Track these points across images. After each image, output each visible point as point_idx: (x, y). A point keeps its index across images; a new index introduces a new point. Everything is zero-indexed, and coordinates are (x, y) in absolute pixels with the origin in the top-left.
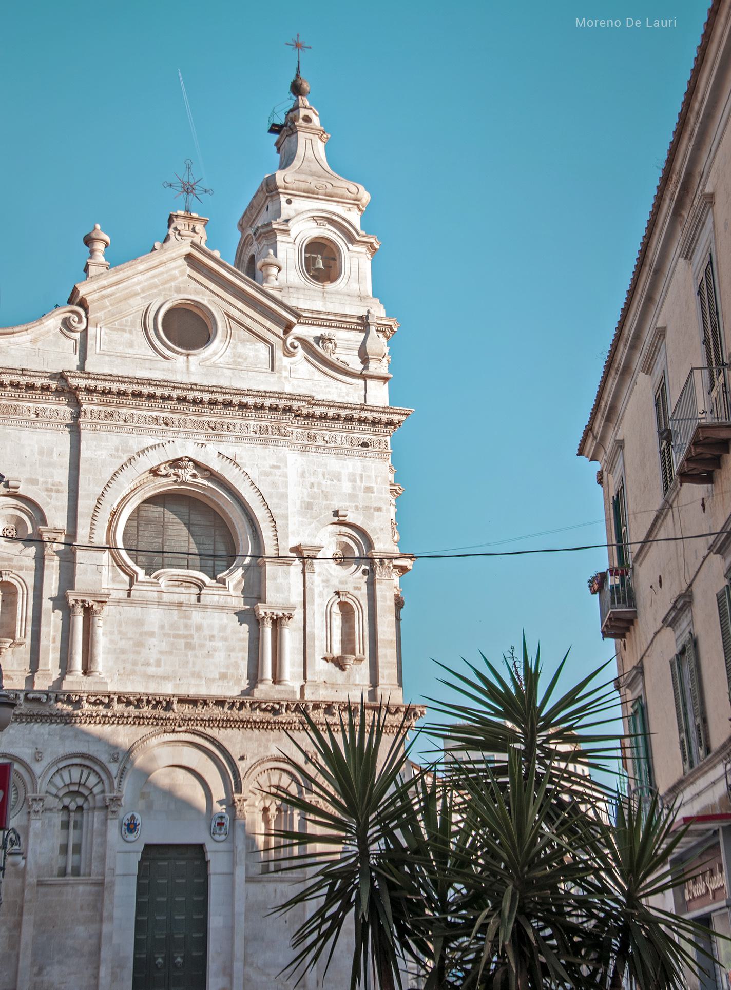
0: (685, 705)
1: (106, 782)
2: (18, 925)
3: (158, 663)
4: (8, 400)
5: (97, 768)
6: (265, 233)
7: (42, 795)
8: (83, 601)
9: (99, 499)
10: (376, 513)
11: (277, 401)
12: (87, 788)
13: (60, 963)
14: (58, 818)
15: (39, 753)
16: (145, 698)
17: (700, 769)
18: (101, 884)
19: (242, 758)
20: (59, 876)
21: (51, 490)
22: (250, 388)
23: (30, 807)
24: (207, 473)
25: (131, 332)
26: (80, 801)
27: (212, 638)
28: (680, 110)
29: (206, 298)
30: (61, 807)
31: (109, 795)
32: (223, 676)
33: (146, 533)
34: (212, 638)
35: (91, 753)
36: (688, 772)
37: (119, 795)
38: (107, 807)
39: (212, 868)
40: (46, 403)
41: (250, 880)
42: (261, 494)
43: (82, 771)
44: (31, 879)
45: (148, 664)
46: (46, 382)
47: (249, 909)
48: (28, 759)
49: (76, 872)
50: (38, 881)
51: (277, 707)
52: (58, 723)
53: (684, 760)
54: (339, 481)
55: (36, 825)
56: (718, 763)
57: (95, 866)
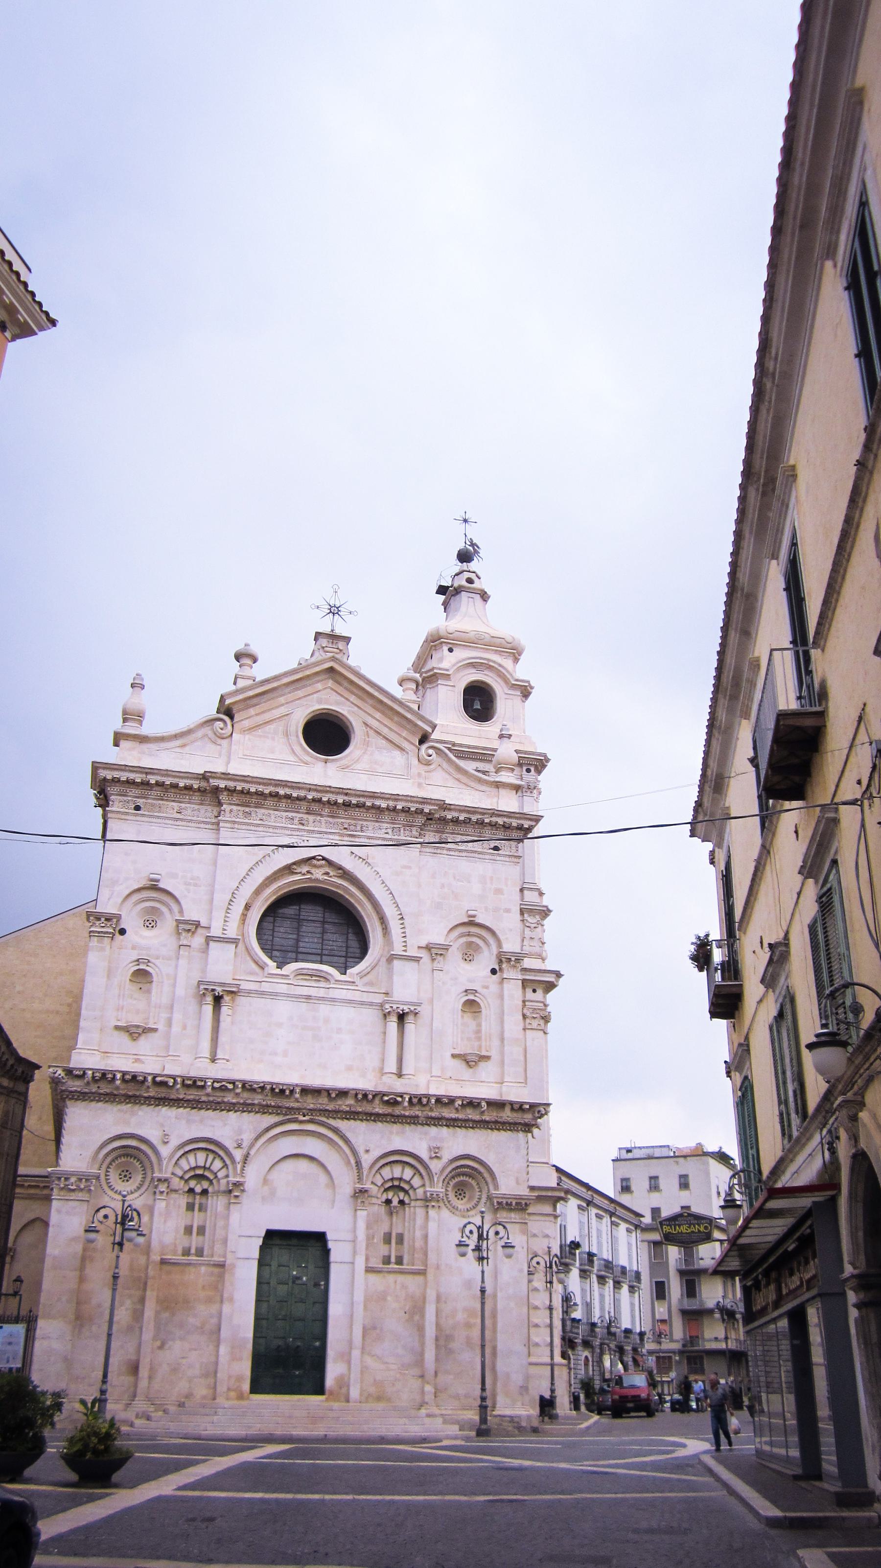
0: (784, 1073)
1: (230, 1167)
2: (142, 1300)
3: (285, 1054)
4: (154, 799)
5: (221, 1153)
6: (428, 677)
7: (168, 1175)
8: (213, 990)
9: (233, 893)
10: (505, 914)
11: (409, 805)
12: (212, 1171)
13: (182, 1339)
14: (183, 1200)
15: (166, 1135)
16: (268, 1087)
17: (798, 1139)
18: (222, 1265)
19: (367, 1151)
20: (183, 1255)
21: (189, 884)
22: (383, 791)
23: (156, 1187)
24: (340, 871)
25: (273, 739)
26: (205, 1184)
27: (339, 1031)
28: (763, 296)
29: (346, 708)
30: (186, 1189)
31: (232, 1179)
32: (349, 1068)
33: (282, 930)
34: (339, 1031)
35: (215, 1138)
36: (787, 1146)
37: (241, 1180)
38: (230, 1191)
39: (333, 1257)
40: (189, 803)
41: (369, 1270)
42: (391, 893)
43: (208, 1155)
44: (156, 1257)
45: (276, 1054)
46: (188, 782)
47: (367, 1300)
48: (155, 1141)
49: (200, 1252)
50: (162, 1259)
51: (399, 1099)
52: (185, 1108)
53: (783, 1134)
54: (469, 882)
55: (161, 1205)
56: (815, 1130)
57: (218, 1248)
